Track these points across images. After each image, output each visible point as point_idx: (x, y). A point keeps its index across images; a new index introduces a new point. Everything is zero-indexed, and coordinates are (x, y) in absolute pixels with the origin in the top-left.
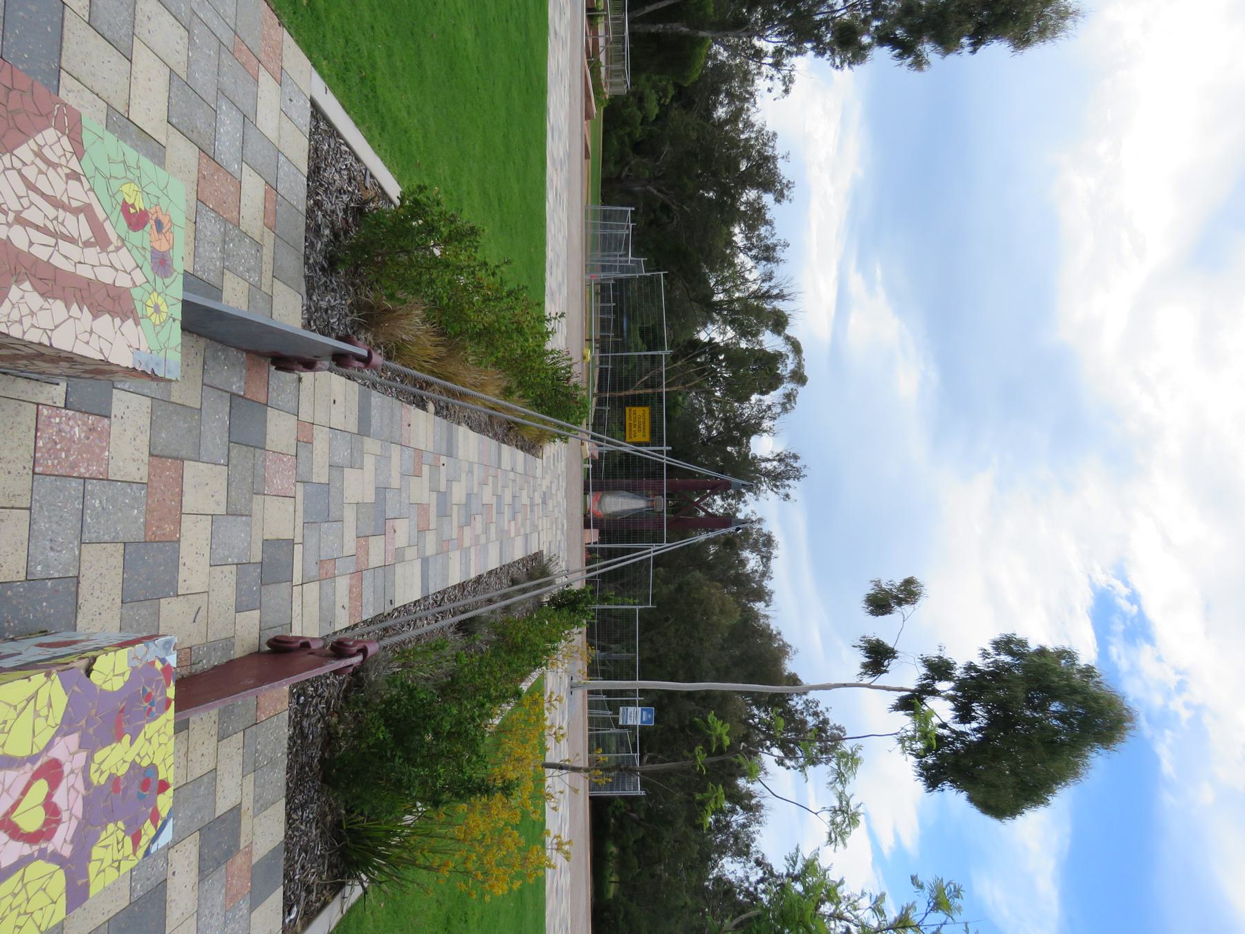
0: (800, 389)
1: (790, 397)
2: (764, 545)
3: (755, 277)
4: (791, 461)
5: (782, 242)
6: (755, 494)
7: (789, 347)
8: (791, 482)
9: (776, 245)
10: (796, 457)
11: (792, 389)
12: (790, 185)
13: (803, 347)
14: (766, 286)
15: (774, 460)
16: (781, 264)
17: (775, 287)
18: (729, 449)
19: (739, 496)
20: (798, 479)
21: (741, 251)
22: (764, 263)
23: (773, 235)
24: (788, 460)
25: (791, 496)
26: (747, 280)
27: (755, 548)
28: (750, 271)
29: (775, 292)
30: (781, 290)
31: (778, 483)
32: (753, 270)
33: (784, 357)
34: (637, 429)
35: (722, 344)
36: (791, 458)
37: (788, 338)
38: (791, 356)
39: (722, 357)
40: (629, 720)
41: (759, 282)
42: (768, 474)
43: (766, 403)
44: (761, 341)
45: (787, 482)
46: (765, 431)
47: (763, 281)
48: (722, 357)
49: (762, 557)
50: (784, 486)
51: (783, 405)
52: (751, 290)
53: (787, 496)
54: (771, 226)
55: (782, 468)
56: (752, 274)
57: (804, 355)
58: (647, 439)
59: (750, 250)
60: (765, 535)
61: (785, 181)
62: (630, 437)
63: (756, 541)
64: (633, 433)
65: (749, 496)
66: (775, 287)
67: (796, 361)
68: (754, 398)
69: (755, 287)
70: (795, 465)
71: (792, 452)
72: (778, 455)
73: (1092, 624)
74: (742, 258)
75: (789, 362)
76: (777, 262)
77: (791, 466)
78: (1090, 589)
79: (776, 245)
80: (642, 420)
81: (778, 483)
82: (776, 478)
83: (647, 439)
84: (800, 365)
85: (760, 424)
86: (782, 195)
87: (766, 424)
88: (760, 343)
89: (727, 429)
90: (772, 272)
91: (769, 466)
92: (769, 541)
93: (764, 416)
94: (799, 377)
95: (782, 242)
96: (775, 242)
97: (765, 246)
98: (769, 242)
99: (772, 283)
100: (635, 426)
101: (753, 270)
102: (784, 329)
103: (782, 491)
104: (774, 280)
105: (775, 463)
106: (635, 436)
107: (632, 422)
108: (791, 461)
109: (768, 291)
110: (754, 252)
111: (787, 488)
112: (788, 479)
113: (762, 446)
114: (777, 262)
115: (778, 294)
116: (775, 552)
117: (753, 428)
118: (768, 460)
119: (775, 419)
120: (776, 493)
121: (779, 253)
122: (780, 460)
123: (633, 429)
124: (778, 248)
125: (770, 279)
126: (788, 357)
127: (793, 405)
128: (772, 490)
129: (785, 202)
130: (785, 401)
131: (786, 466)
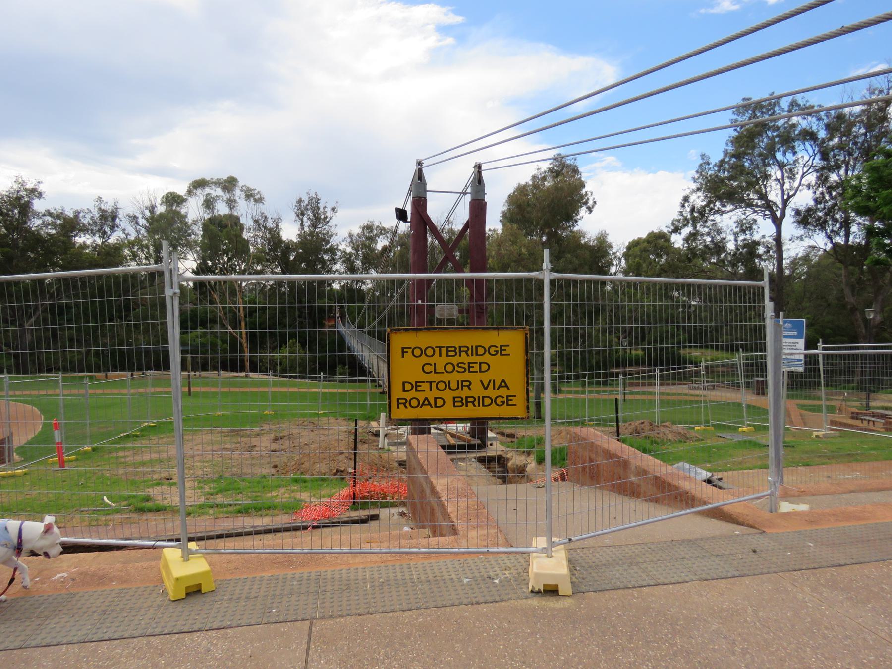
0: (241, 183)
1: (249, 195)
2: (372, 231)
3: (134, 231)
4: (303, 205)
5: (97, 203)
6: (332, 236)
7: (199, 191)
8: (321, 206)
9: (100, 209)
10: (300, 201)
11: (241, 191)
12: (20, 181)
13: (198, 177)
14: (142, 221)
15: (302, 219)
16: (118, 206)
17: (143, 214)
18: (292, 258)
19: (332, 250)
20: (319, 200)
21: (106, 241)
22: (118, 221)
23: (90, 211)
24: (302, 208)
25: (333, 206)
26: (137, 238)
27: (372, 239)
28: (127, 235)
29: (148, 213)
30: (146, 208)
31: (322, 217)
32: (126, 232)
33: (209, 198)
34: (475, 378)
35: (198, 262)
36: (300, 205)
37: (190, 192)
38: (207, 190)
39: (210, 263)
40: (797, 357)
41: (138, 227)
42: (314, 226)
43: (252, 224)
44: (194, 221)
45: (321, 209)
46: (277, 225)
47: (137, 223)
48: (210, 263)
49: (381, 234)
50: (324, 212)
51: (256, 201)
52: (146, 234)
53: (333, 209)
54: (79, 213)
55: (309, 212)
56: (130, 233)
57: (208, 179)
58: (513, 339)
59: (105, 233)
60: (363, 230)
61: (16, 187)
62: (508, 401)
63: (368, 238)
64: (491, 393)
65: (334, 241)
66: (143, 214)
67: (213, 187)
68: (246, 235)
69: (143, 231)
70: (306, 202)
71: (295, 203)
72: (298, 216)
73: (415, 5)
74: (112, 240)
75: (213, 194)
76: (117, 209)
77: (307, 205)
78: (390, 4)
79: (100, 209)
80: (440, 361)
81: (322, 217)
82: (318, 219)
83: (513, 339)
84: (218, 183)
85: (270, 230)
86: (33, 191)
87: (270, 224)
88: (195, 222)
89: (275, 258)
90: (129, 216)
91: (307, 223)
92: (369, 228)
93: (263, 227)
94: (229, 184)
95: (97, 203)
96: (96, 209)
97: (101, 219)
98: (97, 215)
99: (140, 216)
100: (461, 385)
101: (126, 232)
102: (179, 196)
103: (329, 213)
104: (137, 214)
105: (305, 218)
106: (504, 384)
107: (448, 395)
108: (303, 205)
109: (147, 219)
110: (107, 230)
111: (326, 209)
112: (318, 208)
113: (290, 232)
114: (117, 209)
115: (150, 211)
116: (376, 224)
117: (275, 239)
118: (302, 225)
119: (266, 217)
120: (331, 218)
121: (109, 207)
122: (303, 214)
123: (477, 391)
124: (103, 207)
125: (135, 217)
126: (209, 194)
127: (256, 192)
128: (328, 222)
129: (41, 188)
130: (252, 199)
131: (307, 209)
